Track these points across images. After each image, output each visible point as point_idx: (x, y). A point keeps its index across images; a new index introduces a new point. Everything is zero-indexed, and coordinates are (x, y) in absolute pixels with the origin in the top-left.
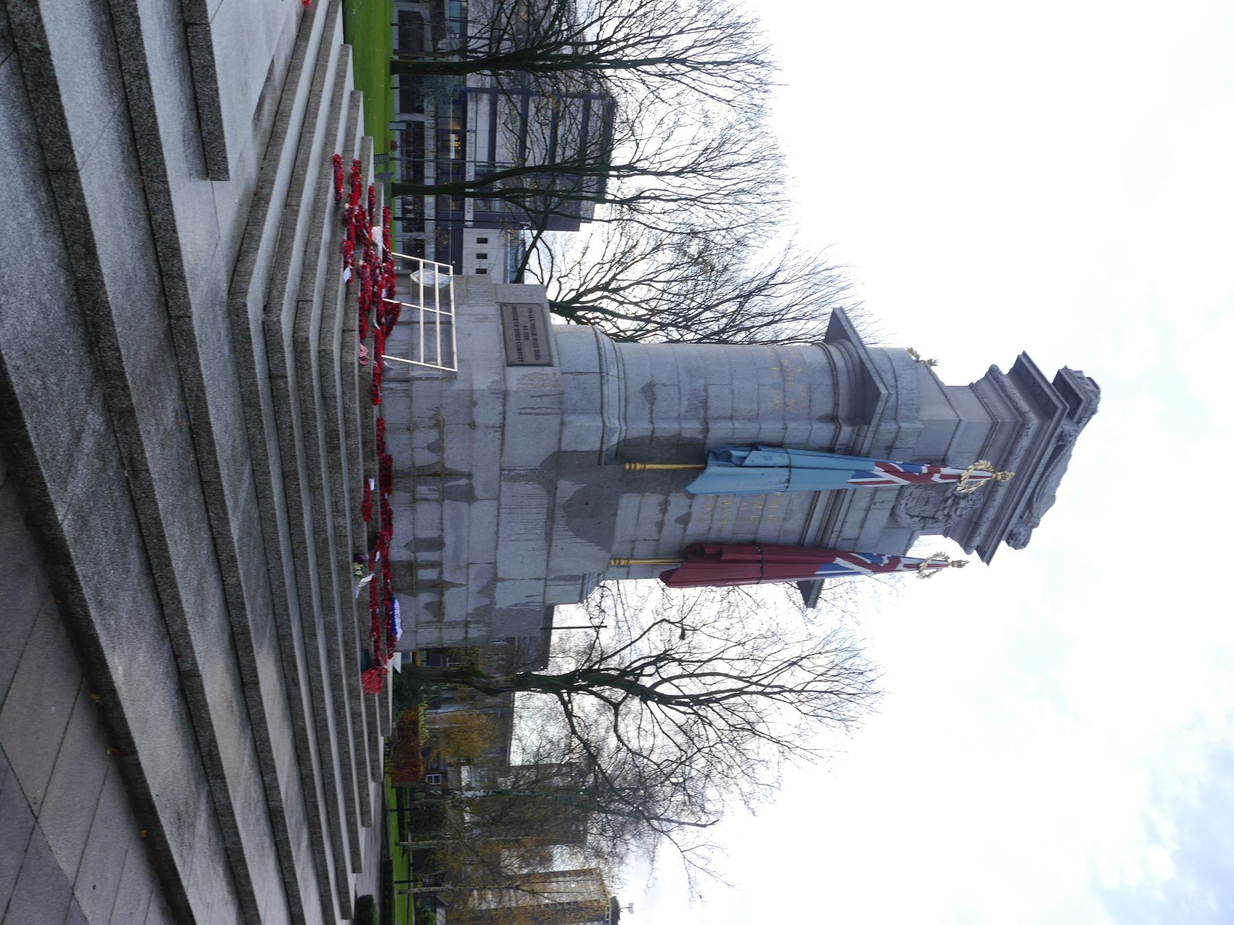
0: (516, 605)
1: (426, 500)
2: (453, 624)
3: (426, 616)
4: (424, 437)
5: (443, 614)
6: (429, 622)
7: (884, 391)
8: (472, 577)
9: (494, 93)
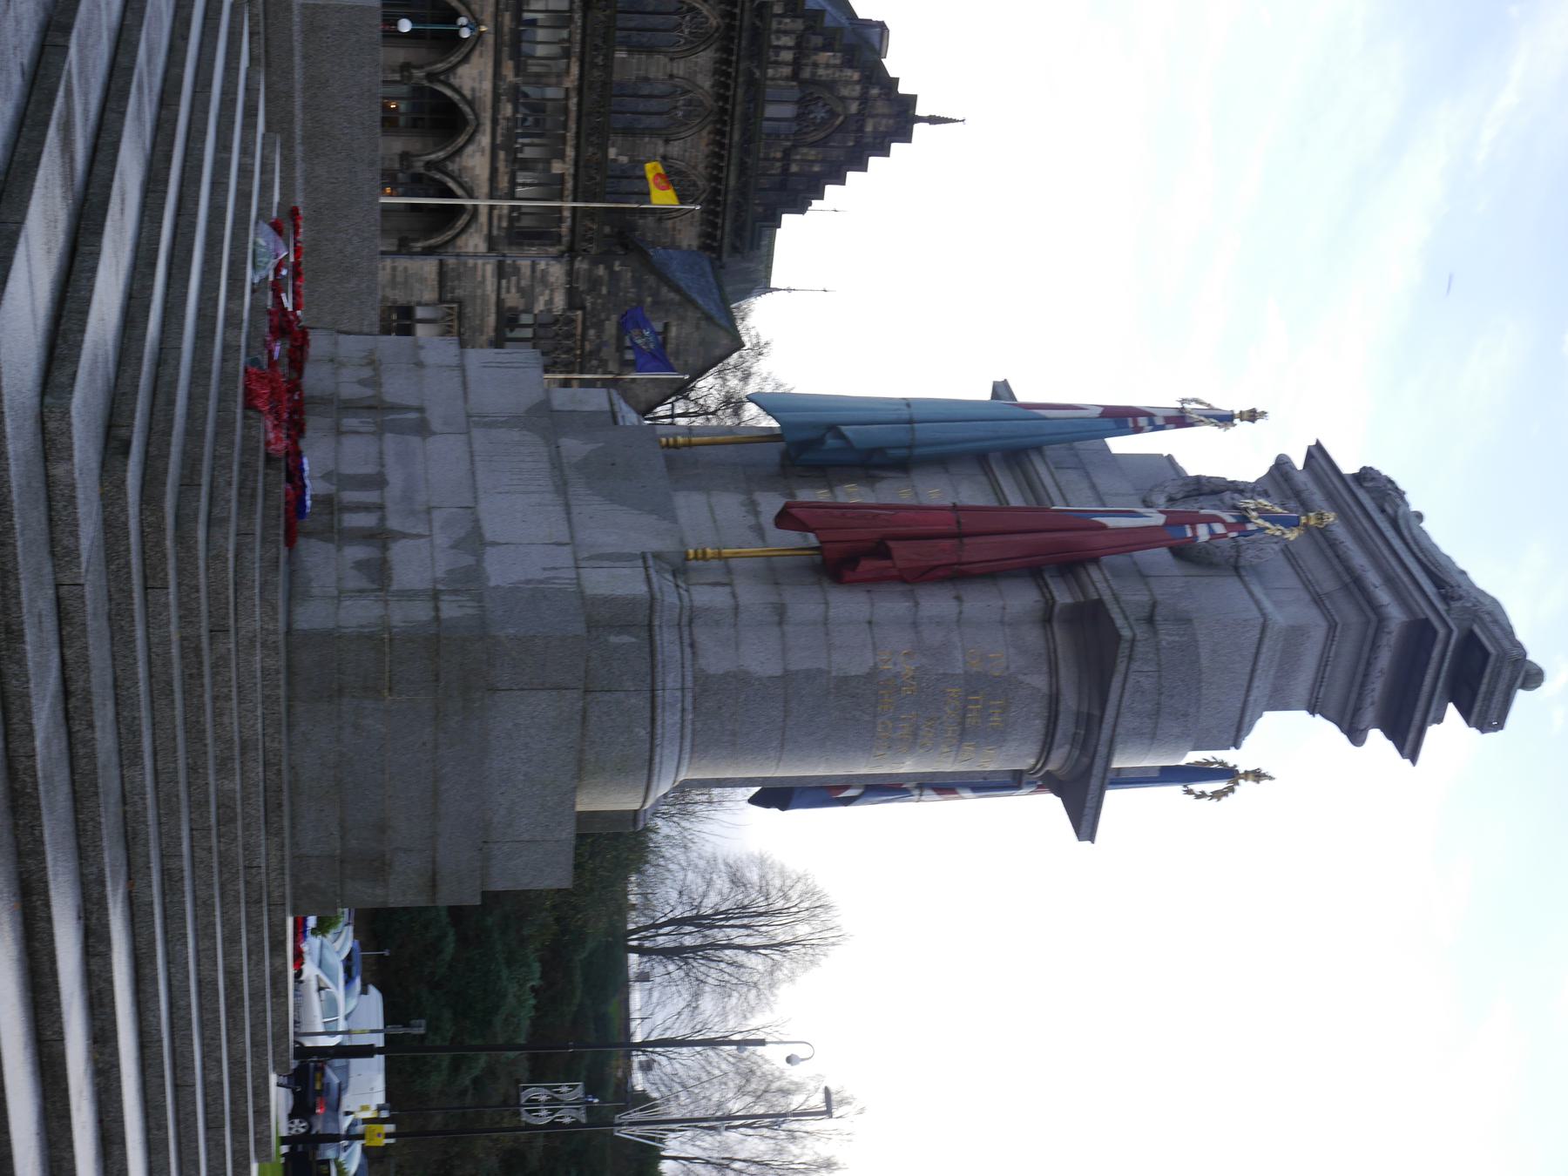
0: (528, 582)
2: (409, 595)
3: (355, 581)
5: (390, 578)
6: (361, 591)
7: (1126, 633)
8: (437, 525)
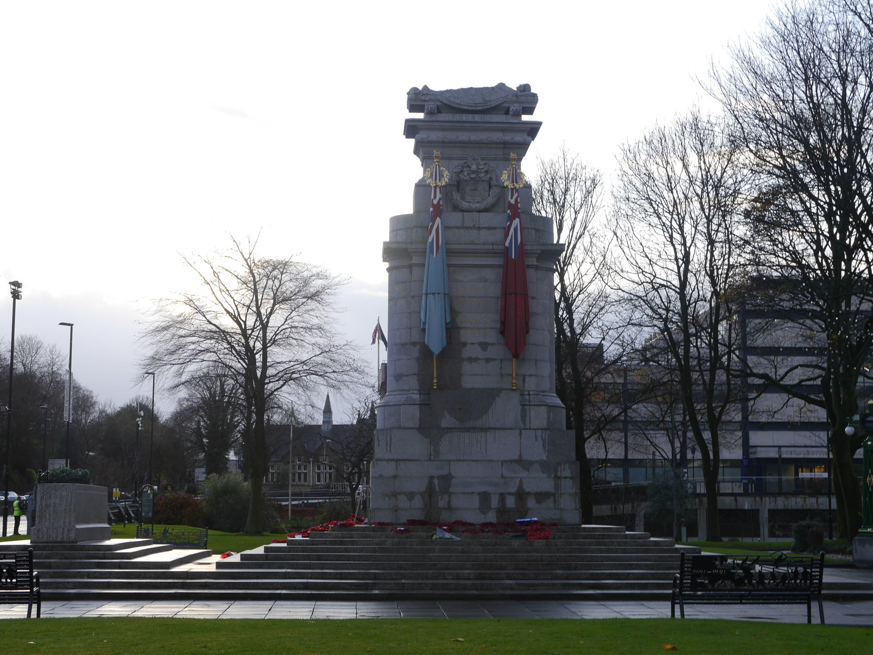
0: (544, 446)
1: (449, 502)
2: (557, 486)
4: (403, 502)
6: (555, 502)
8: (513, 475)
9: (747, 426)
